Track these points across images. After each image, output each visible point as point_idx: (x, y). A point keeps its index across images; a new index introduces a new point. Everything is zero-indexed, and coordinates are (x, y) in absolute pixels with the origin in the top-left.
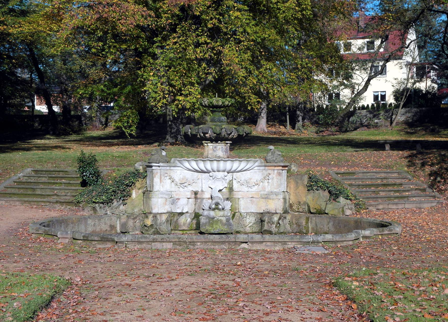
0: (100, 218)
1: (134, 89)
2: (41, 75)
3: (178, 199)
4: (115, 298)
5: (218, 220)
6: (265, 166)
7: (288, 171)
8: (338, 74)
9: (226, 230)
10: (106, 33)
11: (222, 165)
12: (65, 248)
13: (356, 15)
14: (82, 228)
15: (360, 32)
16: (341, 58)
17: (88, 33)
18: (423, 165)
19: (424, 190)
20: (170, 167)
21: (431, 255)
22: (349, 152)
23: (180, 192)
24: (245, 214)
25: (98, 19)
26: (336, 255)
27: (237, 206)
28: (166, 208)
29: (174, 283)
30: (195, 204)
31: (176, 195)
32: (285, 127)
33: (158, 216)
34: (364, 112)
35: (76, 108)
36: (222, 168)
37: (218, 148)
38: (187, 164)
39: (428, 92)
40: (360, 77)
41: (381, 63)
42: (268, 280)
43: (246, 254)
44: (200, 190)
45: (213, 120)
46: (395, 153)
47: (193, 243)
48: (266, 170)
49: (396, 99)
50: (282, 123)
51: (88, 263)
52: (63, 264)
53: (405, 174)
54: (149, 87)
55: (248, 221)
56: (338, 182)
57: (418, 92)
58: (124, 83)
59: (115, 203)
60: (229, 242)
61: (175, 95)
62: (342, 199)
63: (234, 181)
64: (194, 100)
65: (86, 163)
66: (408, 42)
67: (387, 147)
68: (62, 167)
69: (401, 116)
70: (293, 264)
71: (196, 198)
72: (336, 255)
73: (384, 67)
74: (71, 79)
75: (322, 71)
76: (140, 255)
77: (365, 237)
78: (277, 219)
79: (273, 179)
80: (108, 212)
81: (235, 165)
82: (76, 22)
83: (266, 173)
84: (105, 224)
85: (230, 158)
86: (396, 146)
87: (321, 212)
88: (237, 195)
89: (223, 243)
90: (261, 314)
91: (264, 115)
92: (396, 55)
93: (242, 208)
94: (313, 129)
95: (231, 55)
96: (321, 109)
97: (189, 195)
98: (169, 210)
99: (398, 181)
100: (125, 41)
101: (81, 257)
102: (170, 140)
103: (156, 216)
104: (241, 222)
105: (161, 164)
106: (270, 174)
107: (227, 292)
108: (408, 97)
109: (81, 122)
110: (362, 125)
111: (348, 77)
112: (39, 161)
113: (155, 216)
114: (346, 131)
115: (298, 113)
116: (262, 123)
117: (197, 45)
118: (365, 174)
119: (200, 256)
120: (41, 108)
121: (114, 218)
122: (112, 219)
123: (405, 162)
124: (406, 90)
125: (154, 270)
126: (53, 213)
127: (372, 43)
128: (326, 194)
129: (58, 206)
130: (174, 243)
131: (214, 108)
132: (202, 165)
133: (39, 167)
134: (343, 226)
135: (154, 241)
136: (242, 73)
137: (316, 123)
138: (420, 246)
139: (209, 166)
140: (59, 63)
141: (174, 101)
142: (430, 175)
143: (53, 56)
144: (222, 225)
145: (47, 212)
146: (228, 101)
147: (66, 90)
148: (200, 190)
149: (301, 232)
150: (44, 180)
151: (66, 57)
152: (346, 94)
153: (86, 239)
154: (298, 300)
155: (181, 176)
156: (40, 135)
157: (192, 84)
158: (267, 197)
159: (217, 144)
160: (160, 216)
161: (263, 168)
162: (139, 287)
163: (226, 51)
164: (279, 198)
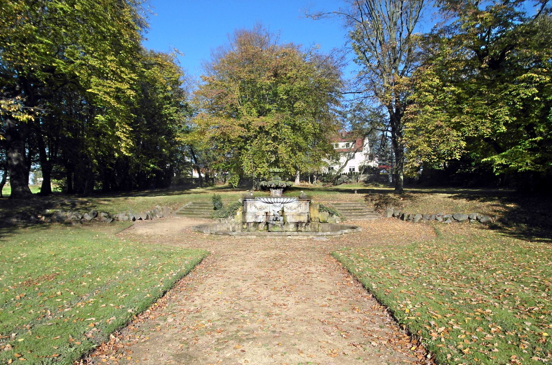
0: (222, 224)
1: (237, 165)
2: (196, 160)
4: (230, 260)
7: (310, 203)
8: (333, 158)
10: (224, 139)
11: (279, 200)
12: (207, 238)
13: (341, 131)
14: (215, 229)
15: (343, 139)
16: (334, 151)
17: (216, 140)
18: (372, 200)
19: (372, 212)
21: (376, 241)
22: (338, 194)
25: (222, 133)
26: (332, 241)
29: (257, 254)
34: (345, 176)
35: (211, 174)
36: (279, 201)
38: (262, 199)
39: (374, 167)
40: (343, 159)
41: (353, 154)
42: (301, 252)
43: (290, 241)
45: (274, 179)
46: (360, 194)
47: (265, 236)
49: (360, 170)
50: (307, 181)
51: (218, 244)
52: (206, 245)
54: (244, 164)
56: (333, 208)
57: (369, 167)
58: (233, 162)
59: (229, 218)
60: (282, 235)
61: (256, 168)
62: (334, 216)
64: (265, 170)
65: (216, 199)
66: (365, 144)
67: (356, 191)
68: (206, 201)
69: (363, 177)
70: (312, 246)
72: (332, 241)
73: (354, 155)
74: (209, 161)
75: (325, 156)
76: (241, 241)
77: (345, 233)
81: (285, 200)
82: (211, 135)
83: (299, 203)
85: (283, 196)
86: (360, 191)
87: (325, 222)
88: (286, 214)
89: (280, 236)
90: (297, 267)
91: (298, 177)
92: (359, 150)
94: (321, 184)
95: (282, 150)
96: (325, 175)
99: (361, 208)
100: (233, 143)
101: (215, 242)
102: (254, 189)
107: (282, 258)
108: (365, 169)
109: (213, 181)
110: (344, 182)
111: (338, 159)
112: (195, 198)
114: (337, 185)
116: (297, 180)
117: (267, 144)
119: (269, 242)
120: (196, 175)
121: (229, 225)
123: (364, 199)
124: (364, 166)
125: (248, 248)
126: (202, 222)
127: (349, 144)
128: (328, 213)
129: (203, 219)
130: (257, 236)
131: (275, 173)
132: (269, 200)
133: (195, 201)
134: (335, 228)
135: (248, 235)
136: (287, 158)
137: (323, 181)
138: (370, 237)
139: (273, 200)
140: (204, 154)
141: (256, 170)
142: (375, 205)
143: (201, 151)
145: (199, 222)
146: (281, 170)
147: (207, 167)
149: (315, 231)
150: (197, 207)
151: (207, 151)
152: (336, 168)
153: (216, 234)
154: (315, 261)
156: (194, 187)
157: (264, 162)
158: (300, 215)
162: (241, 255)
163: (280, 147)
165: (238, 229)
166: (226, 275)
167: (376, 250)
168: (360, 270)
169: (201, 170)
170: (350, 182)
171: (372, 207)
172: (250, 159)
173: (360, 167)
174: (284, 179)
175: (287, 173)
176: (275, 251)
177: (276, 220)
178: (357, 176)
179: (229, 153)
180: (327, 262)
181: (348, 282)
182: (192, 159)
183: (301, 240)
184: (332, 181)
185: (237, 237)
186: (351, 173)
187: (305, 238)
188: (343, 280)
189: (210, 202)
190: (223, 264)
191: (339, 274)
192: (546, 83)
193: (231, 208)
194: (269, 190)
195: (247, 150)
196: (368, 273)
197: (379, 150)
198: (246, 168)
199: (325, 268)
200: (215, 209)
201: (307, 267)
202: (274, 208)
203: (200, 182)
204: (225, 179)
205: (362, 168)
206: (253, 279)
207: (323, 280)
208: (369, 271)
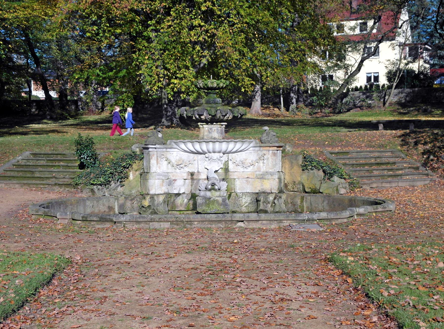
1: (129, 73)
2: (37, 61)
3: (175, 180)
4: (115, 276)
5: (214, 200)
7: (283, 152)
9: (222, 210)
12: (65, 228)
14: (81, 209)
16: (335, 40)
18: (416, 144)
19: (417, 168)
20: (166, 148)
21: (424, 231)
23: (177, 173)
24: (241, 194)
26: (331, 232)
27: (233, 186)
28: (164, 189)
30: (192, 185)
31: (173, 176)
32: (279, 108)
33: (155, 197)
34: (357, 93)
35: (72, 92)
37: (213, 130)
38: (183, 146)
39: (420, 73)
40: (353, 58)
41: (374, 45)
42: (265, 256)
43: (242, 233)
44: (196, 171)
45: (208, 102)
46: (389, 132)
47: (190, 222)
49: (389, 80)
50: (276, 105)
51: (88, 242)
52: (63, 243)
53: (399, 153)
55: (244, 201)
56: (333, 162)
57: (410, 72)
60: (226, 221)
61: (170, 79)
62: (336, 178)
63: (229, 162)
65: (83, 146)
67: (381, 126)
69: (394, 97)
70: (289, 242)
71: (192, 179)
72: (331, 232)
73: (377, 48)
74: (66, 63)
76: (138, 235)
77: (359, 215)
78: (273, 199)
79: (268, 159)
81: (231, 146)
82: (71, 6)
83: (261, 153)
85: (225, 139)
86: (388, 125)
87: (315, 192)
88: (232, 176)
89: (220, 221)
90: (258, 289)
92: (389, 36)
93: (238, 188)
94: (307, 110)
95: (223, 35)
97: (185, 176)
98: (166, 191)
99: (392, 160)
101: (81, 236)
102: (166, 123)
103: (153, 198)
104: (237, 202)
105: (157, 146)
106: (265, 155)
107: (225, 268)
109: (77, 106)
110: (355, 106)
111: (341, 58)
112: (38, 144)
114: (340, 112)
116: (257, 104)
117: (192, 28)
120: (39, 93)
121: (112, 200)
122: (110, 201)
123: (399, 141)
124: (399, 70)
125: (153, 248)
126: (53, 195)
127: (365, 24)
128: (321, 173)
129: (57, 189)
130: (172, 223)
132: (198, 147)
133: (37, 151)
134: (338, 204)
135: (152, 221)
137: (311, 104)
139: (204, 147)
141: (168, 84)
142: (423, 154)
143: (48, 41)
144: (218, 205)
145: (46, 195)
146: (222, 83)
148: (196, 171)
149: (296, 211)
152: (340, 75)
153: (85, 219)
154: (294, 275)
155: (178, 158)
156: (38, 119)
157: (187, 68)
158: (262, 177)
159: (213, 126)
160: (158, 197)
162: (139, 265)
163: (219, 33)
164: (274, 177)
165: (133, 209)
166: (106, 307)
167: (426, 250)
168: (392, 292)
169: (49, 83)
170: (369, 107)
171: (416, 156)
172: (155, 61)
173: (389, 72)
174: (227, 102)
175: (236, 89)
176: (211, 255)
177: (213, 188)
178: (383, 92)
179: (110, 47)
180: (322, 276)
181: (366, 317)
182: (27, 58)
183: (266, 231)
184: (331, 104)
185: (129, 226)
186: (371, 85)
187: (274, 226)
188: (356, 314)
189: (71, 152)
190: (98, 283)
191: (346, 302)
193: (116, 164)
194: (198, 126)
195: (149, 40)
196: (410, 299)
197: (431, 35)
198: (148, 79)
199: (316, 289)
200: (82, 166)
201: (277, 288)
202: (206, 164)
203: (48, 110)
204: (103, 103)
205: (395, 74)
206: (163, 314)
207: (314, 314)
208: (411, 294)
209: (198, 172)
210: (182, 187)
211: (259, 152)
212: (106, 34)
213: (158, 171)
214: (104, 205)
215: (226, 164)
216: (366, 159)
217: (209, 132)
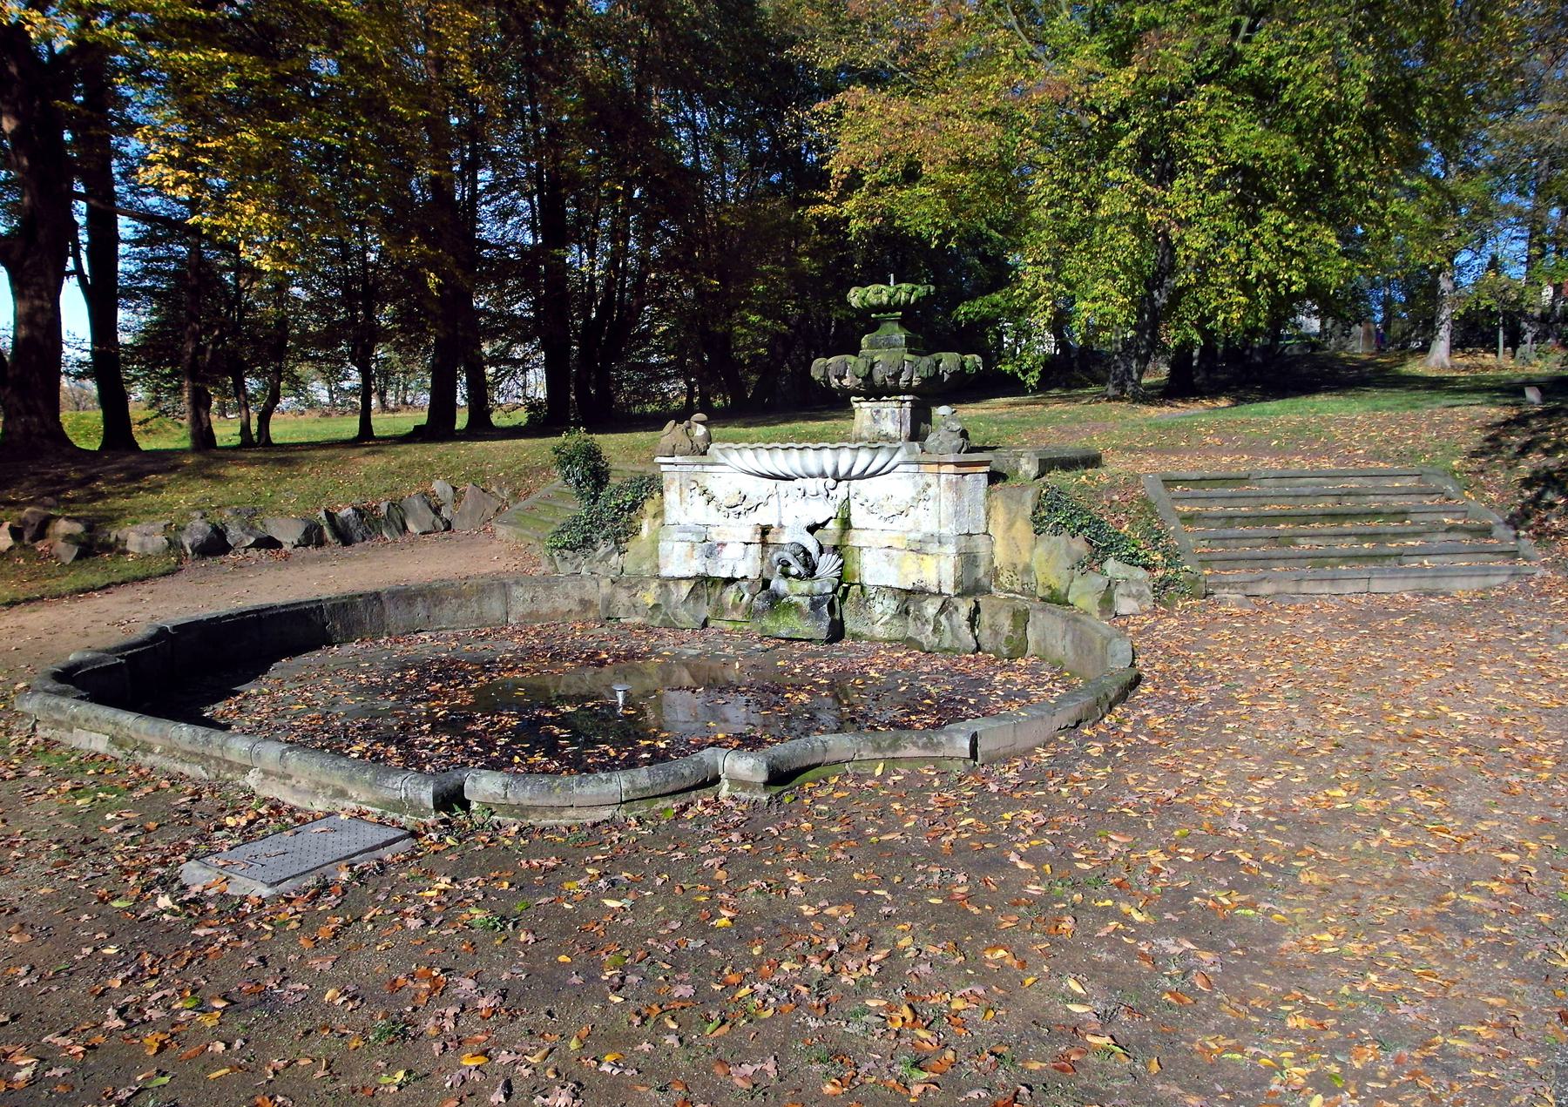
5: (790, 605)
6: (918, 463)
19: (1486, 532)
27: (856, 567)
28: (695, 567)
30: (762, 559)
32: (1496, 353)
33: (671, 585)
48: (923, 474)
53: (1439, 481)
55: (878, 608)
71: (764, 543)
79: (938, 498)
80: (584, 571)
84: (567, 596)
88: (856, 539)
97: (749, 534)
98: (702, 570)
105: (678, 459)
113: (665, 583)
115: (1524, 325)
118: (1286, 481)
142: (1527, 483)
158: (918, 549)
161: (913, 468)
171: (1501, 487)
192: (140, 363)
209: (781, 526)
210: (740, 561)
211: (918, 477)
212: (129, 150)
213: (684, 521)
214: (567, 596)
215: (846, 504)
216: (1300, 500)
217: (875, 421)
